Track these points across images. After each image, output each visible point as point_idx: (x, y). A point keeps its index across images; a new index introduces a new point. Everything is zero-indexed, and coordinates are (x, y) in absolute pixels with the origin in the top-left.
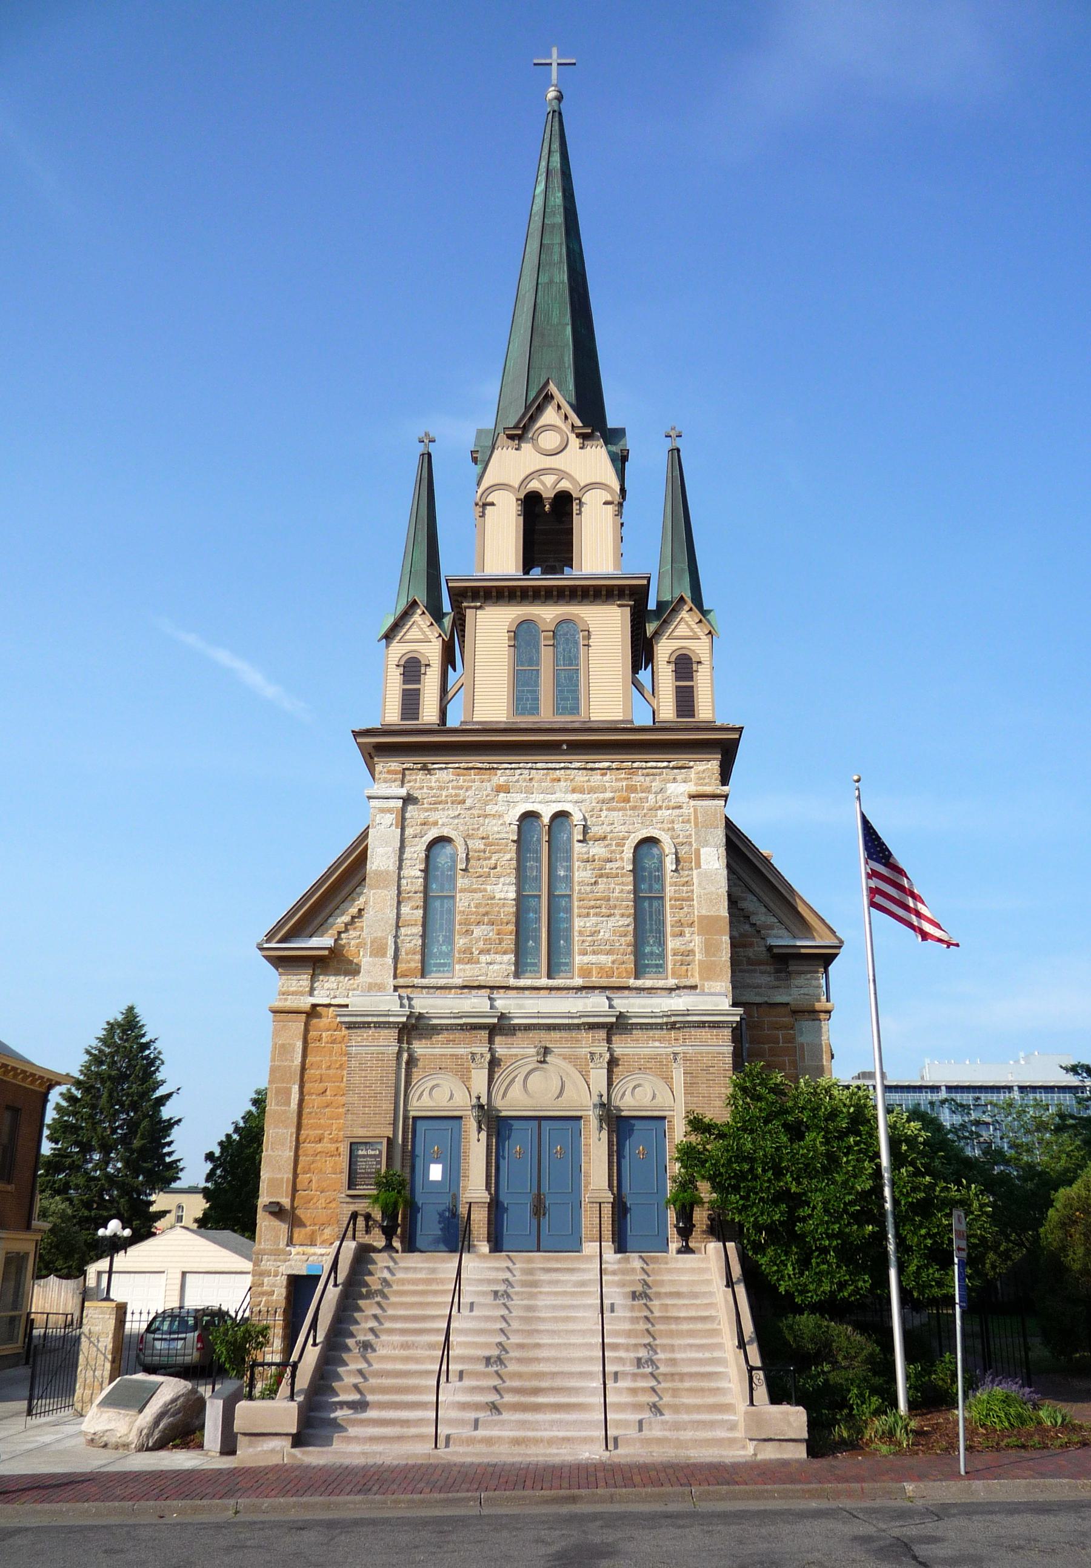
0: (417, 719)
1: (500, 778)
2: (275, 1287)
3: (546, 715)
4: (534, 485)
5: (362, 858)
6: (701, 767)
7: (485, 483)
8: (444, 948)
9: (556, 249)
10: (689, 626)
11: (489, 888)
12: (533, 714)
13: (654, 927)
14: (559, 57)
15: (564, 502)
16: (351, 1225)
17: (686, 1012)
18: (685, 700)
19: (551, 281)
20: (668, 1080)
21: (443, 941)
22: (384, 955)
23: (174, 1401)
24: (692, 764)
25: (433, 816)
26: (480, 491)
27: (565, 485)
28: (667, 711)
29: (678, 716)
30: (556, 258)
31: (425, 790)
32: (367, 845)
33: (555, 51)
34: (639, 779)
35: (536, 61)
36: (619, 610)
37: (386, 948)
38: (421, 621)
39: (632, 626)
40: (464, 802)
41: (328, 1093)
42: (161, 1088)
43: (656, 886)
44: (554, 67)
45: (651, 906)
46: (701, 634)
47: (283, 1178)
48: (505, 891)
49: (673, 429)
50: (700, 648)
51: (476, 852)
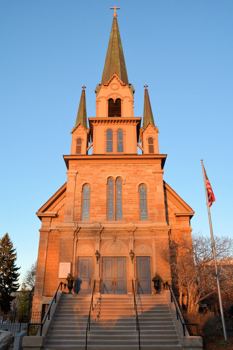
0: (80, 153)
1: (102, 168)
2: (39, 307)
3: (115, 152)
4: (111, 97)
5: (65, 190)
6: (156, 165)
7: (98, 97)
8: (87, 213)
9: (116, 46)
10: (152, 130)
11: (99, 196)
12: (111, 152)
13: (145, 207)
14: (116, 7)
15: (119, 100)
16: (60, 285)
17: (155, 227)
18: (151, 149)
19: (115, 53)
20: (151, 246)
21: (87, 211)
22: (70, 215)
23: (5, 338)
24: (153, 164)
25: (84, 178)
26: (97, 98)
27: (119, 97)
28: (147, 152)
29: (149, 153)
30: (116, 48)
31: (82, 171)
32: (66, 187)
33: (115, 6)
34: (140, 168)
35: (111, 8)
36: (133, 126)
37: (71, 213)
38: (81, 129)
39: (137, 128)
40: (93, 174)
41: (55, 253)
42: (17, 264)
43: (145, 196)
44: (115, 9)
45: (143, 202)
46: (155, 132)
47: (42, 277)
48: (104, 197)
49: (146, 85)
50: (154, 136)
51: (96, 187)
